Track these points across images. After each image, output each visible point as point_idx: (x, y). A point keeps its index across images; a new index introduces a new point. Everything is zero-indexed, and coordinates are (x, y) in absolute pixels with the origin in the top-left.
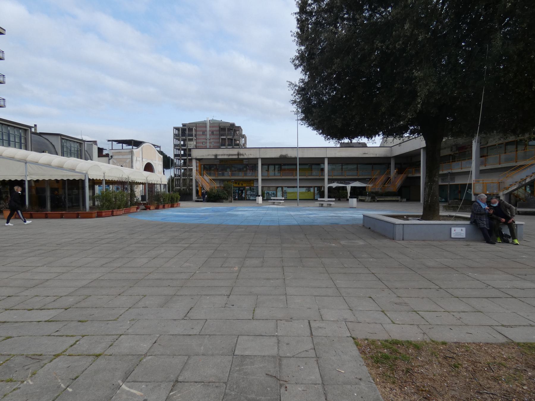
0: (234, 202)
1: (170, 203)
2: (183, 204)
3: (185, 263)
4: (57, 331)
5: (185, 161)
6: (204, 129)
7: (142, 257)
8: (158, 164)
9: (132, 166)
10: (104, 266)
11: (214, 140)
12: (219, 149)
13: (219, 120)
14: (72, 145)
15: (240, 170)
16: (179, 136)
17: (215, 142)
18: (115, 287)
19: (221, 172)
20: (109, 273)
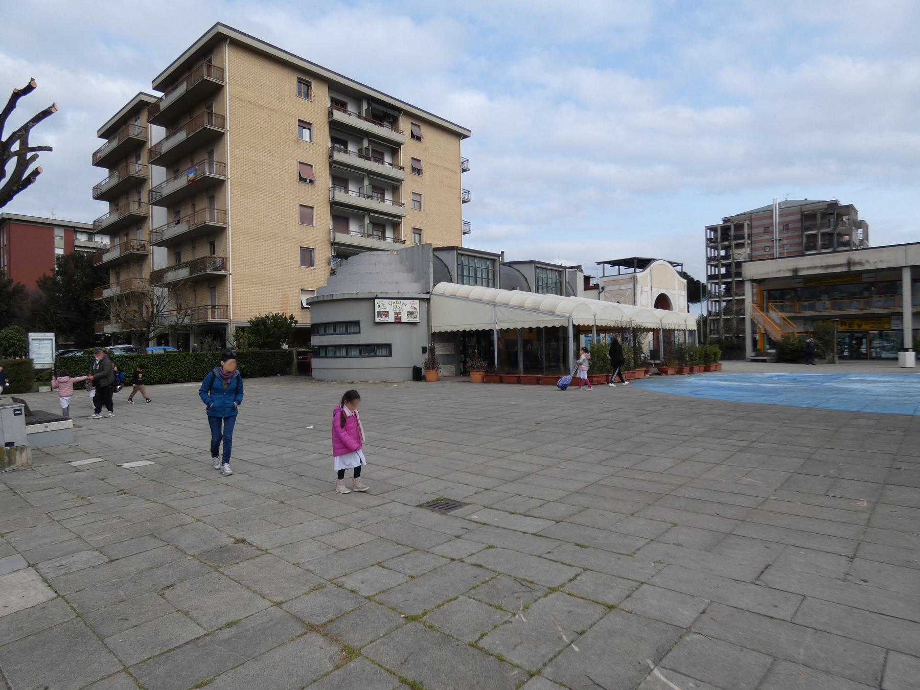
0: (839, 363)
1: (701, 363)
2: (726, 365)
3: (743, 476)
4: (549, 552)
5: (729, 286)
6: (767, 222)
7: (662, 455)
8: (678, 296)
9: (635, 302)
10: (603, 463)
11: (790, 241)
12: (802, 257)
13: (801, 200)
14: (550, 276)
15: (853, 296)
16: (716, 241)
17: (791, 245)
18: (624, 500)
19: (806, 303)
20: (612, 475)
